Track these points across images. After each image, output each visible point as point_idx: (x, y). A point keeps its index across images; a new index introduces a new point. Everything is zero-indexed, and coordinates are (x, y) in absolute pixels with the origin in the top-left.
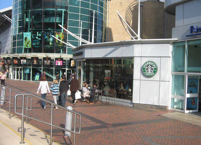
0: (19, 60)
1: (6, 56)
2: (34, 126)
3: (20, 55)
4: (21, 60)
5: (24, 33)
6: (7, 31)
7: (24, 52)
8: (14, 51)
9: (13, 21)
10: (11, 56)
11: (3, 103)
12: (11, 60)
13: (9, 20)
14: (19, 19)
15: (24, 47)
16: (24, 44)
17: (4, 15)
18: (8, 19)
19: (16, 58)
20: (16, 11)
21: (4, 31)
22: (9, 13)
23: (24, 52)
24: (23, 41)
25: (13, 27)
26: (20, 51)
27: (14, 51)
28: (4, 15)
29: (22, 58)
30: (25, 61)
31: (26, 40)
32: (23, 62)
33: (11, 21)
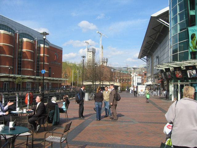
0: (184, 72)
1: (163, 68)
2: (54, 48)
3: (184, 64)
4: (188, 72)
5: (190, 29)
6: (164, 41)
7: (191, 58)
8: (175, 58)
9: (171, 25)
10: (172, 66)
11: (40, 101)
12: (171, 73)
13: (166, 24)
14: (181, 30)
15: (191, 50)
16: (191, 45)
17: (160, 19)
18: (164, 23)
19: (179, 69)
20: (175, 11)
21: (161, 43)
22: (165, 16)
23: (191, 58)
24: (188, 41)
25: (172, 34)
26: (185, 58)
27: (175, 58)
28: (160, 19)
29: (188, 68)
30: (194, 72)
31: (194, 39)
32: (190, 74)
33: (168, 26)
